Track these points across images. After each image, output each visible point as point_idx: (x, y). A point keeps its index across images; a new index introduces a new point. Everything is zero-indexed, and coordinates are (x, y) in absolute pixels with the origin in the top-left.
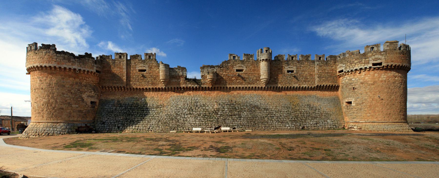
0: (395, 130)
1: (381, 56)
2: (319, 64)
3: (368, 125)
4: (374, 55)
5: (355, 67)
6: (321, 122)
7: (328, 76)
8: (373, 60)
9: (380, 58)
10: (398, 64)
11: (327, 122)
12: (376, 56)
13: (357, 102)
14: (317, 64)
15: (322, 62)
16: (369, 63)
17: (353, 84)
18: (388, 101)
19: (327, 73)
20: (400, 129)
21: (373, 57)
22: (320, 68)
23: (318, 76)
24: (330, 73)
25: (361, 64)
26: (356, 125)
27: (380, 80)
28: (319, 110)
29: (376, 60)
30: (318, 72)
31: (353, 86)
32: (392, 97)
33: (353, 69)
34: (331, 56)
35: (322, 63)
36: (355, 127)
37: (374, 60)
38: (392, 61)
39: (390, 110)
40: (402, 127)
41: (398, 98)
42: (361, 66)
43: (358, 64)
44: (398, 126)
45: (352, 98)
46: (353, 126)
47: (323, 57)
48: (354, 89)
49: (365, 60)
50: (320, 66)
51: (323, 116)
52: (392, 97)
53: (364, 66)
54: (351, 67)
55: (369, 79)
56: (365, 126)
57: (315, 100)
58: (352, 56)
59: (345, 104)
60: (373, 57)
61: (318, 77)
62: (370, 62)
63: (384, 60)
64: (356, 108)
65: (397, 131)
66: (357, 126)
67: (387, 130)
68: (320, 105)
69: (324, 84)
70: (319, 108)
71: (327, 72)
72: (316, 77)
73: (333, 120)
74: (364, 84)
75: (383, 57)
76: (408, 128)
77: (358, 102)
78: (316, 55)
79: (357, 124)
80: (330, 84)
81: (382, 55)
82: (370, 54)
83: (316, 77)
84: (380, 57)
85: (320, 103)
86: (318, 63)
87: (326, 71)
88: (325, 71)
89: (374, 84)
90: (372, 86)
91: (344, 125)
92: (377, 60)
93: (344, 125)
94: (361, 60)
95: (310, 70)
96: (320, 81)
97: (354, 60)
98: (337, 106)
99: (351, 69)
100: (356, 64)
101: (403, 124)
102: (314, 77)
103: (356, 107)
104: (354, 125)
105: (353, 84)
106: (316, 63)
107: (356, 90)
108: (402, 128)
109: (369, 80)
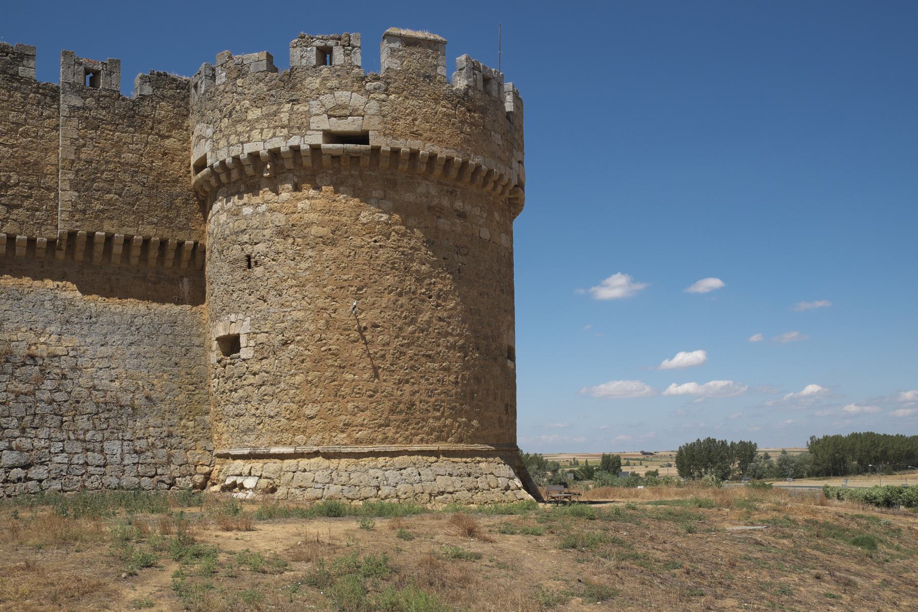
0: (430, 495)
1: (364, 99)
2: (84, 108)
3: (305, 471)
4: (332, 90)
5: (248, 141)
6: (62, 451)
7: (137, 188)
8: (326, 112)
9: (357, 110)
10: (442, 153)
11: (102, 451)
12: (343, 96)
13: (262, 338)
14: (73, 109)
15: (105, 102)
16: (308, 128)
17: (245, 238)
18: (404, 338)
19: (132, 165)
20: (458, 485)
21: (328, 100)
22: (91, 133)
23: (71, 176)
24: (151, 169)
25: (275, 127)
26: (253, 472)
27: (364, 220)
28: (64, 377)
29: (340, 117)
30: (73, 157)
31: (249, 249)
32: (424, 317)
33: (242, 153)
34: (159, 75)
35: (104, 108)
36: (249, 483)
37: (330, 117)
38: (416, 135)
39: (413, 384)
40: (469, 475)
41: (449, 323)
42: (274, 135)
43: (262, 129)
44: (449, 470)
45: (241, 316)
46: (241, 475)
47: (110, 74)
48: (249, 267)
49: (292, 109)
50: (87, 118)
51: (86, 417)
52: (424, 317)
53: (287, 138)
54: (233, 139)
55: (313, 209)
56: (291, 474)
57: (50, 323)
58: (239, 82)
59: (215, 355)
60: (328, 100)
61: (75, 186)
62: (315, 122)
63: (376, 120)
64: (255, 374)
65: (440, 497)
66: (260, 477)
67: (393, 494)
68: (76, 353)
69: (113, 230)
70: (66, 371)
71: (131, 161)
72: (64, 181)
73: (141, 444)
74: (290, 240)
75: (373, 106)
76: (502, 482)
77: (265, 340)
78: (65, 54)
79: (257, 465)
80: (148, 230)
81: (368, 92)
82: (313, 82)
83: (64, 181)
84: (357, 100)
85: (77, 341)
86: (78, 102)
87: (128, 157)
88: (118, 154)
89: (333, 243)
90: (328, 251)
91: (210, 473)
92: (346, 117)
93: (207, 469)
94: (275, 108)
95: (25, 134)
96: (84, 212)
97: (247, 103)
98: (184, 362)
99: (233, 154)
100: (252, 125)
101: (479, 462)
102: (48, 181)
103: (256, 367)
104: (247, 472)
105: (245, 238)
106: (68, 100)
107: (258, 271)
108: (469, 482)
109: (313, 216)
